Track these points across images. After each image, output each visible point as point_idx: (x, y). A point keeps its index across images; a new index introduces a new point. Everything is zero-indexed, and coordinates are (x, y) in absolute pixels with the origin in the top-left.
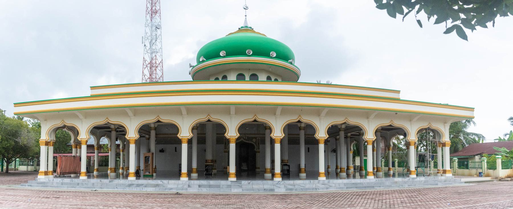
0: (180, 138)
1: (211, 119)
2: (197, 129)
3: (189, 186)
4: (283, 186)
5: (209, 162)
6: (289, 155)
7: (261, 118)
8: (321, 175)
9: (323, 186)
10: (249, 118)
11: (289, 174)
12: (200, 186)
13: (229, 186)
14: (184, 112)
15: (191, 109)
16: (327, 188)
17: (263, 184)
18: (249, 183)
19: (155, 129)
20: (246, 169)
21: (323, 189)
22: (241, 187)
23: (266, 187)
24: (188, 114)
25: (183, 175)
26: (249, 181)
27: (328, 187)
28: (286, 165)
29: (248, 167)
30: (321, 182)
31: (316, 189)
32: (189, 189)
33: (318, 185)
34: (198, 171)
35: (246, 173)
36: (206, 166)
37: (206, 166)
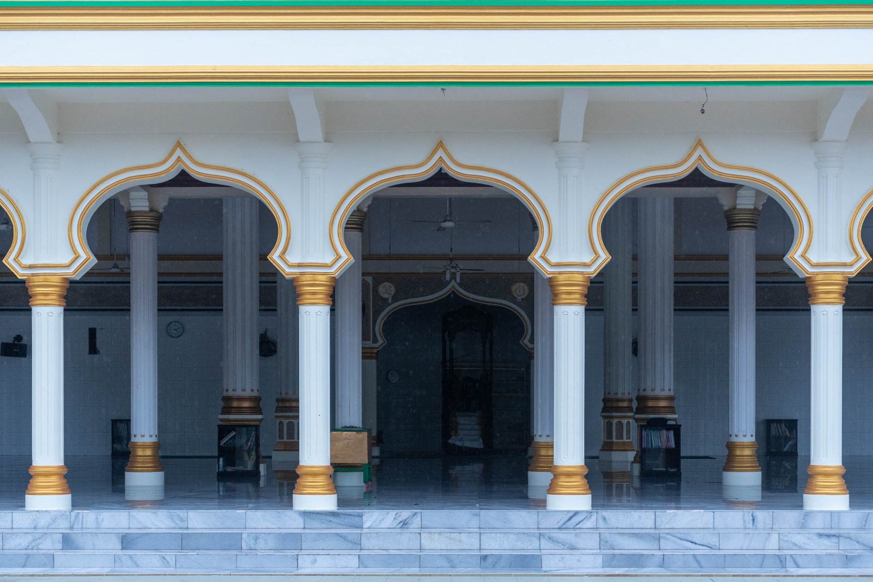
0: (21, 273)
1: (197, 171)
2: (155, 228)
3: (68, 542)
4: (590, 541)
5: (240, 410)
6: (676, 364)
7: (475, 161)
8: (820, 481)
9: (826, 546)
10: (410, 162)
11: (677, 476)
12: (127, 541)
13: (291, 542)
14: (310, 126)
15: (348, 106)
16: (848, 560)
17: (481, 530)
18: (404, 524)
19: (156, 221)
20: (478, 444)
21: (819, 560)
22: (357, 544)
23: (494, 544)
24: (60, 137)
25: (40, 481)
26: (405, 514)
27: (855, 549)
28: (660, 424)
29: (487, 435)
30: (818, 524)
31: (781, 561)
32: (62, 557)
33: (799, 539)
34: (164, 459)
35: (477, 468)
36: (223, 430)
37: (223, 430)
